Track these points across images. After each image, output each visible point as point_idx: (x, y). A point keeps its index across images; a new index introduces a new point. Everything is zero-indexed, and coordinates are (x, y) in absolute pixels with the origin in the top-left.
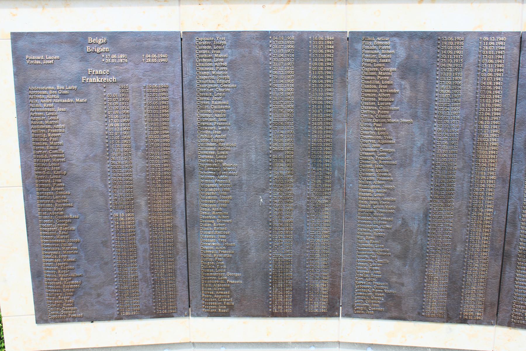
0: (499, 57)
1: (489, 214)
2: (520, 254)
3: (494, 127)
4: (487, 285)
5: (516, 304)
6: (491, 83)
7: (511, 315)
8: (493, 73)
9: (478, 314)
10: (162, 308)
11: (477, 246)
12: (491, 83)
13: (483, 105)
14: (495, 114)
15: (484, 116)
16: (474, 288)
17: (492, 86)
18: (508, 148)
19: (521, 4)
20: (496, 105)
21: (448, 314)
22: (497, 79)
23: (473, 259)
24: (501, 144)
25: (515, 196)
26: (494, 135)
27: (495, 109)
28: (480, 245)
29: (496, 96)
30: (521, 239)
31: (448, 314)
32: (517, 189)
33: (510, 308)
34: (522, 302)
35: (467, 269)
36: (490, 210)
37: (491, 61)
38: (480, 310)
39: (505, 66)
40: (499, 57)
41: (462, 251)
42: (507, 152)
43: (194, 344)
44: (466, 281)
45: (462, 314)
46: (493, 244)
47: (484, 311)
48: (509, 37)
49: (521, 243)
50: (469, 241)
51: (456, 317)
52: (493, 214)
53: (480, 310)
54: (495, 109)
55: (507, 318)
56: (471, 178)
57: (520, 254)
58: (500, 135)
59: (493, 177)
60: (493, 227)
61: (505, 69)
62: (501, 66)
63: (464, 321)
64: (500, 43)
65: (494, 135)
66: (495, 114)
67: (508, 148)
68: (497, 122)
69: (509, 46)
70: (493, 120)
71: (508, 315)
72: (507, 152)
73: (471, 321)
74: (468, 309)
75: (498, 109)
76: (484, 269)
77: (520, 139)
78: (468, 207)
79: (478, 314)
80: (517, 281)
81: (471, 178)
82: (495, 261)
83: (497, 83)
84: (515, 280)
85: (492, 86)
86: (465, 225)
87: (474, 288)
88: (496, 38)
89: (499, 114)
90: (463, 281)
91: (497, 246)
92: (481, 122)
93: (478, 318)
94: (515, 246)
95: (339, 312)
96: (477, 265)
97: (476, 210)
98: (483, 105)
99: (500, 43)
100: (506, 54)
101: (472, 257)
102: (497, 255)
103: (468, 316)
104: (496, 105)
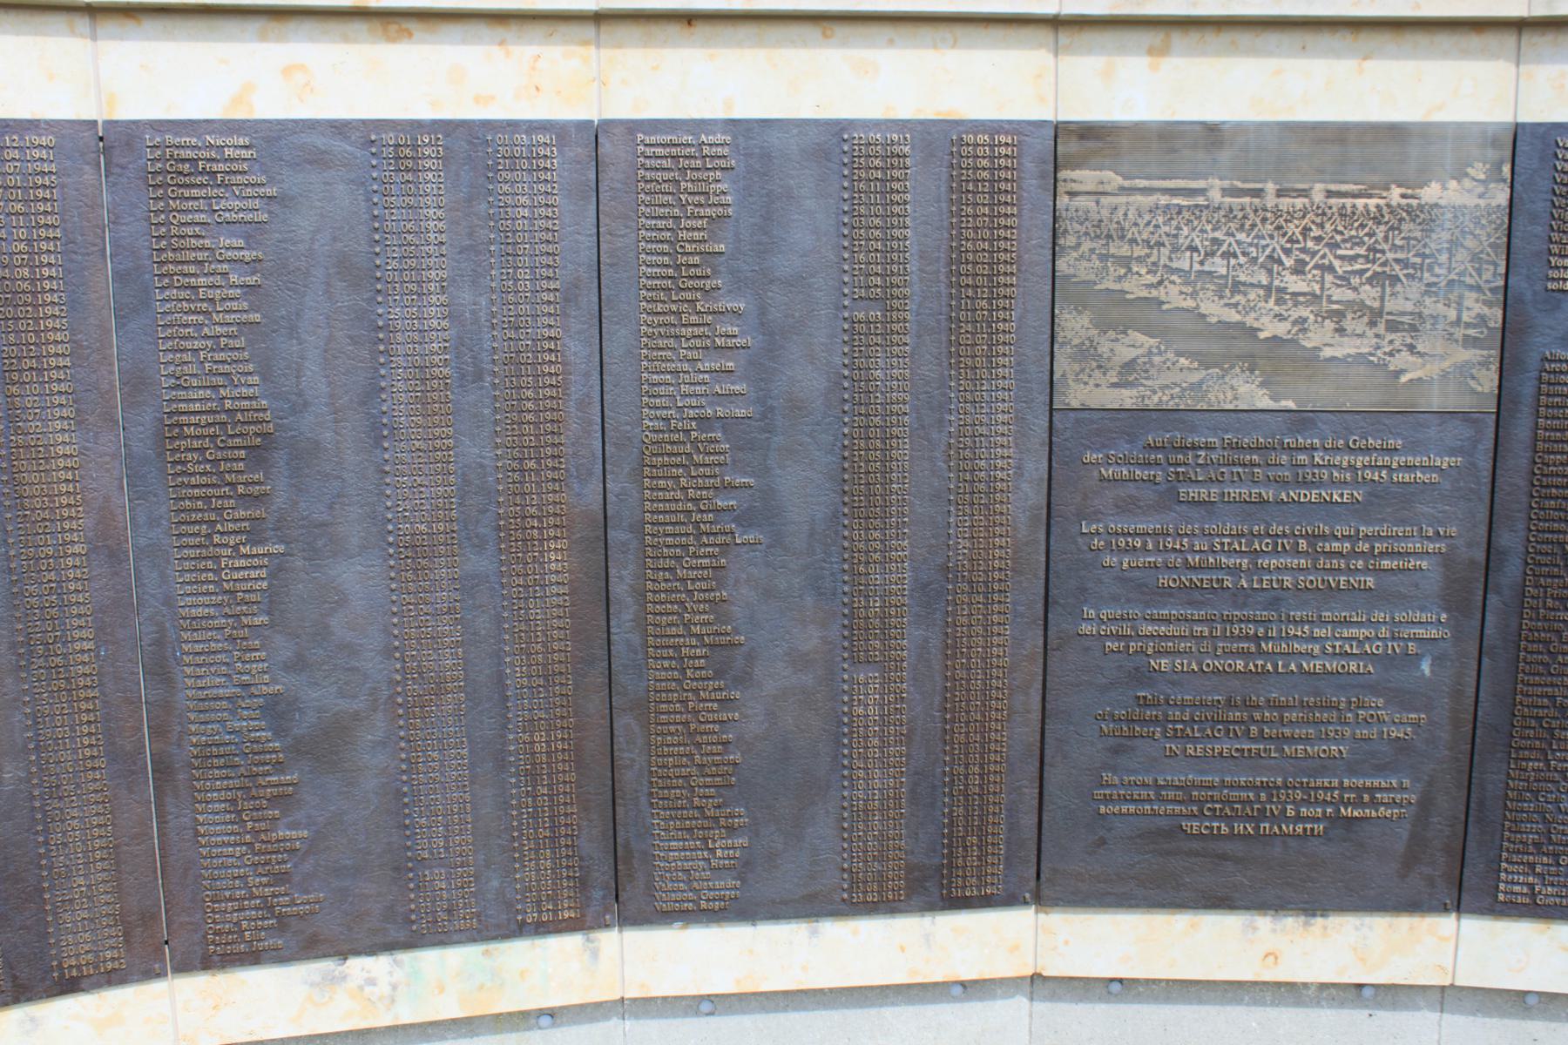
0: (41, 193)
1: (86, 658)
2: (196, 757)
3: (57, 400)
4: (117, 864)
5: (213, 902)
6: (26, 272)
7: (205, 937)
8: (29, 241)
9: (109, 954)
10: (615, 889)
11: (66, 755)
12: (26, 272)
13: (12, 337)
14: (53, 362)
15: (20, 371)
16: (81, 881)
17: (33, 281)
18: (107, 459)
19: (88, 42)
20: (52, 336)
21: (15, 977)
22: (45, 259)
23: (61, 798)
24: (87, 449)
25: (152, 596)
26: (58, 425)
27: (52, 349)
28: (75, 751)
29: (49, 310)
30: (192, 716)
31: (15, 977)
32: (154, 575)
33: (198, 916)
34: (227, 894)
35: (46, 831)
36: (87, 645)
37: (19, 207)
38: (112, 942)
39: (63, 220)
40: (41, 193)
41: (20, 779)
42: (108, 470)
43: (553, 1015)
44: (50, 868)
45: (60, 966)
46: (113, 744)
47: (127, 941)
48: (63, 137)
49: (193, 728)
50: (37, 747)
51: (43, 980)
52: (98, 656)
53: (112, 942)
54: (52, 349)
55: (197, 948)
56: (9, 559)
57: (196, 757)
58: (79, 423)
59: (77, 549)
60: (103, 693)
61: (65, 230)
62: (50, 220)
63: (69, 985)
64: (37, 154)
65: (58, 425)
66: (53, 362)
67: (107, 459)
68: (63, 387)
69: (69, 163)
70: (51, 381)
71: (197, 937)
72: (108, 470)
73: (94, 979)
74: (75, 948)
75: (60, 349)
76: (102, 820)
77: (141, 429)
78: (13, 646)
79: (109, 954)
80: (203, 836)
81: (9, 559)
82: (131, 791)
83: (46, 272)
84: (197, 834)
85: (33, 281)
86: (15, 700)
87: (81, 881)
88: (22, 138)
89: (67, 361)
90: (41, 867)
91: (128, 747)
92: (14, 389)
93: (110, 966)
94: (180, 739)
95: (163, 961)
96: (75, 813)
97: (41, 649)
98: (12, 337)
99: (37, 154)
100: (63, 186)
101: (55, 792)
102: (133, 773)
103: (79, 967)
104: (52, 336)
